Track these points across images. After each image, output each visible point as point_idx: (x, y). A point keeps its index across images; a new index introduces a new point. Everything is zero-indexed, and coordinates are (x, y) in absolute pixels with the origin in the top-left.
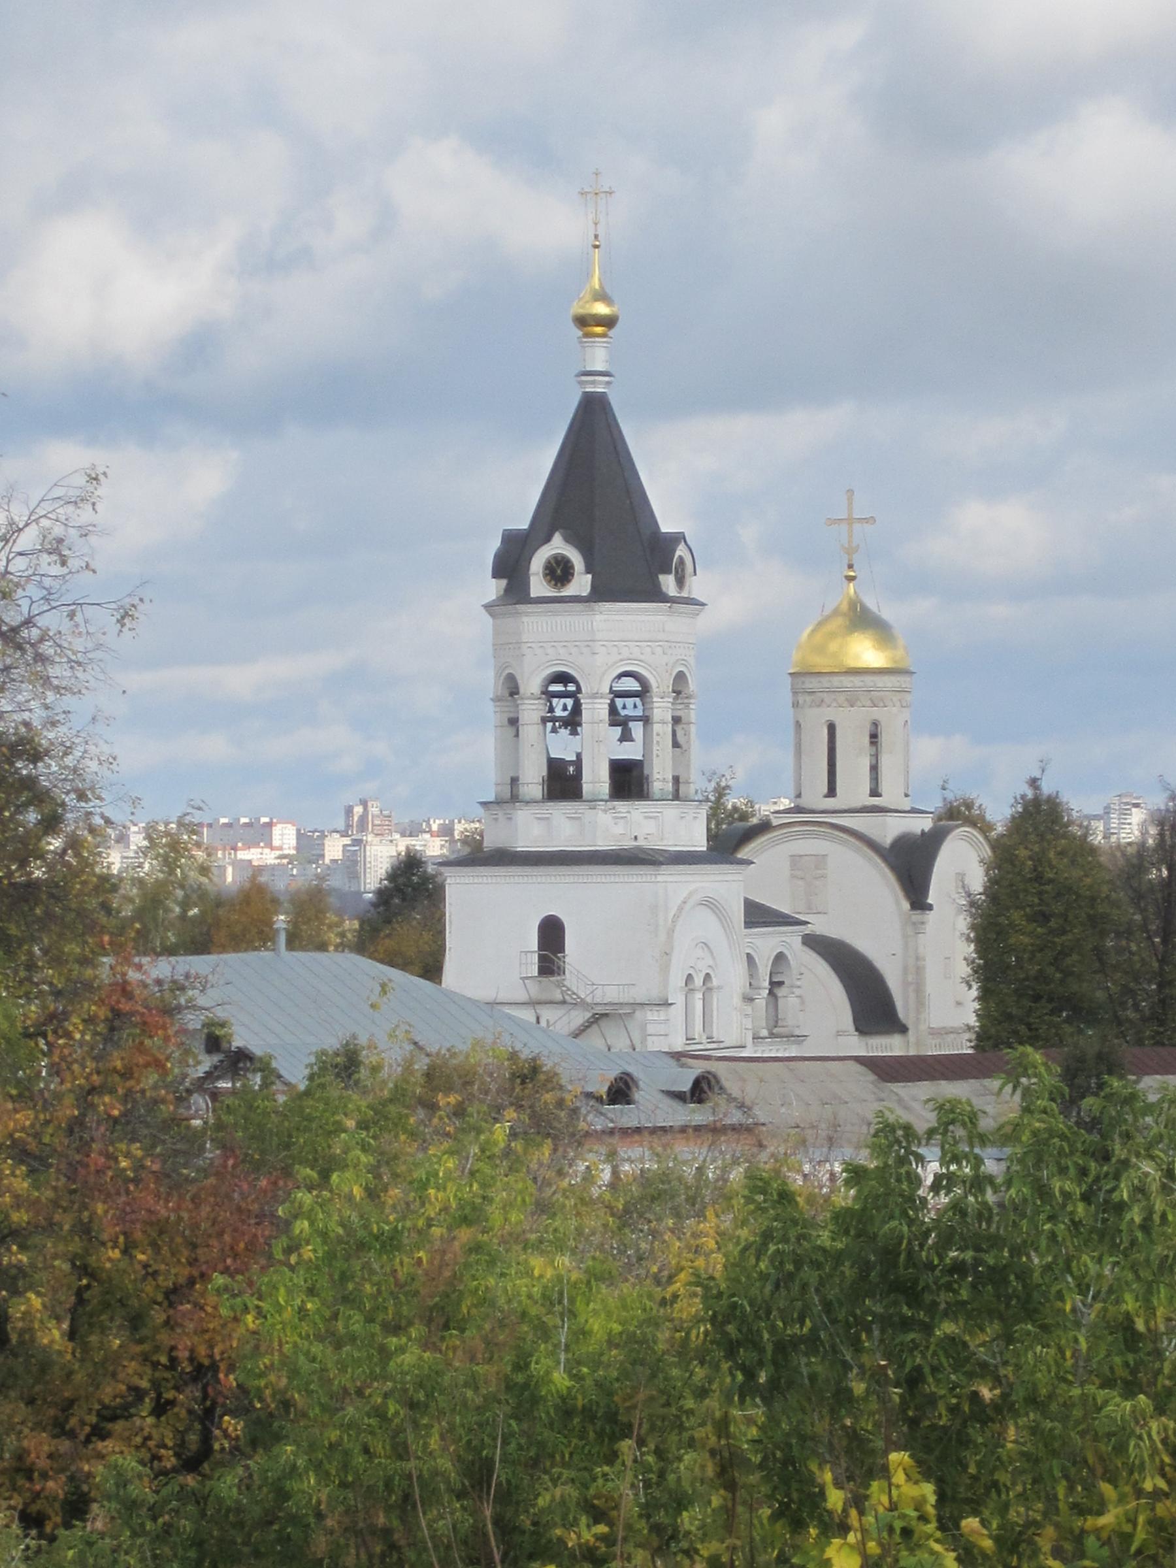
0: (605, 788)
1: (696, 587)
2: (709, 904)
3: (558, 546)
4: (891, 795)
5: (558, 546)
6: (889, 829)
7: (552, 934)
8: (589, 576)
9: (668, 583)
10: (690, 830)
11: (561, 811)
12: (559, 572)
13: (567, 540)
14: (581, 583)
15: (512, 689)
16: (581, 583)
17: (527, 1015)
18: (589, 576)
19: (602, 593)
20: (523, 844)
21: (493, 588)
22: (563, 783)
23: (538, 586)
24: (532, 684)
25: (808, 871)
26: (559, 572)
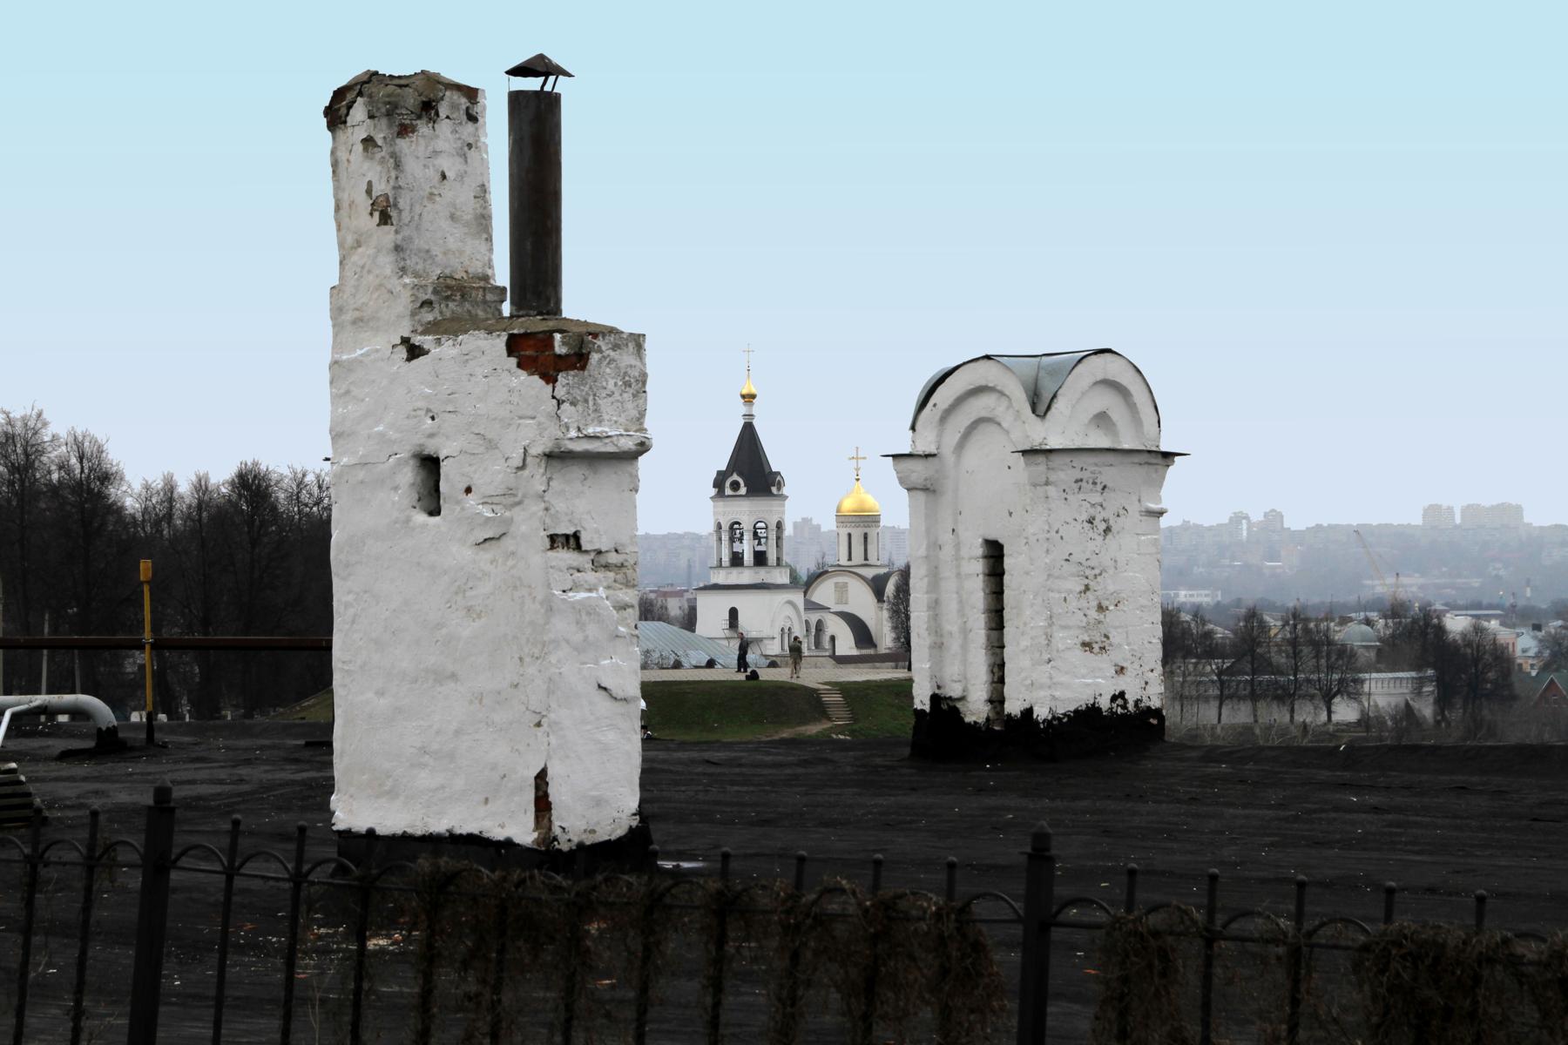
1: (785, 491)
2: (790, 602)
4: (872, 560)
5: (735, 477)
6: (870, 573)
7: (733, 613)
8: (602, 791)
9: (774, 490)
10: (782, 577)
11: (735, 571)
12: (735, 486)
15: (719, 526)
16: (743, 490)
17: (725, 643)
18: (602, 791)
20: (1054, 443)
21: (713, 492)
23: (728, 491)
24: (725, 527)
25: (842, 589)
26: (735, 486)
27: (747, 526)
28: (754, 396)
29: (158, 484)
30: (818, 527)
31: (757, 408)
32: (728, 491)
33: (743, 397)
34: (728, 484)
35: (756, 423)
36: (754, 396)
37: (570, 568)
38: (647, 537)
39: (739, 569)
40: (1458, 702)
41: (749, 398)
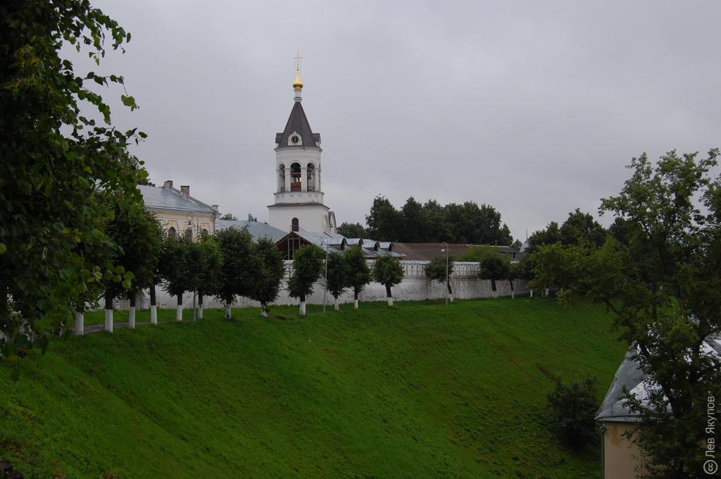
0: (290, 190)
3: (295, 134)
5: (295, 134)
7: (295, 221)
9: (317, 143)
11: (296, 194)
12: (295, 140)
13: (297, 132)
14: (300, 143)
15: (282, 167)
16: (300, 143)
19: (304, 146)
21: (276, 145)
22: (296, 187)
23: (290, 143)
24: (288, 166)
26: (295, 140)
27: (304, 166)
28: (301, 86)
29: (574, 213)
30: (690, 194)
31: (303, 94)
32: (290, 143)
33: (295, 86)
34: (290, 138)
35: (302, 103)
36: (301, 86)
37: (117, 206)
38: (537, 240)
39: (299, 193)
40: (639, 269)
41: (298, 87)
